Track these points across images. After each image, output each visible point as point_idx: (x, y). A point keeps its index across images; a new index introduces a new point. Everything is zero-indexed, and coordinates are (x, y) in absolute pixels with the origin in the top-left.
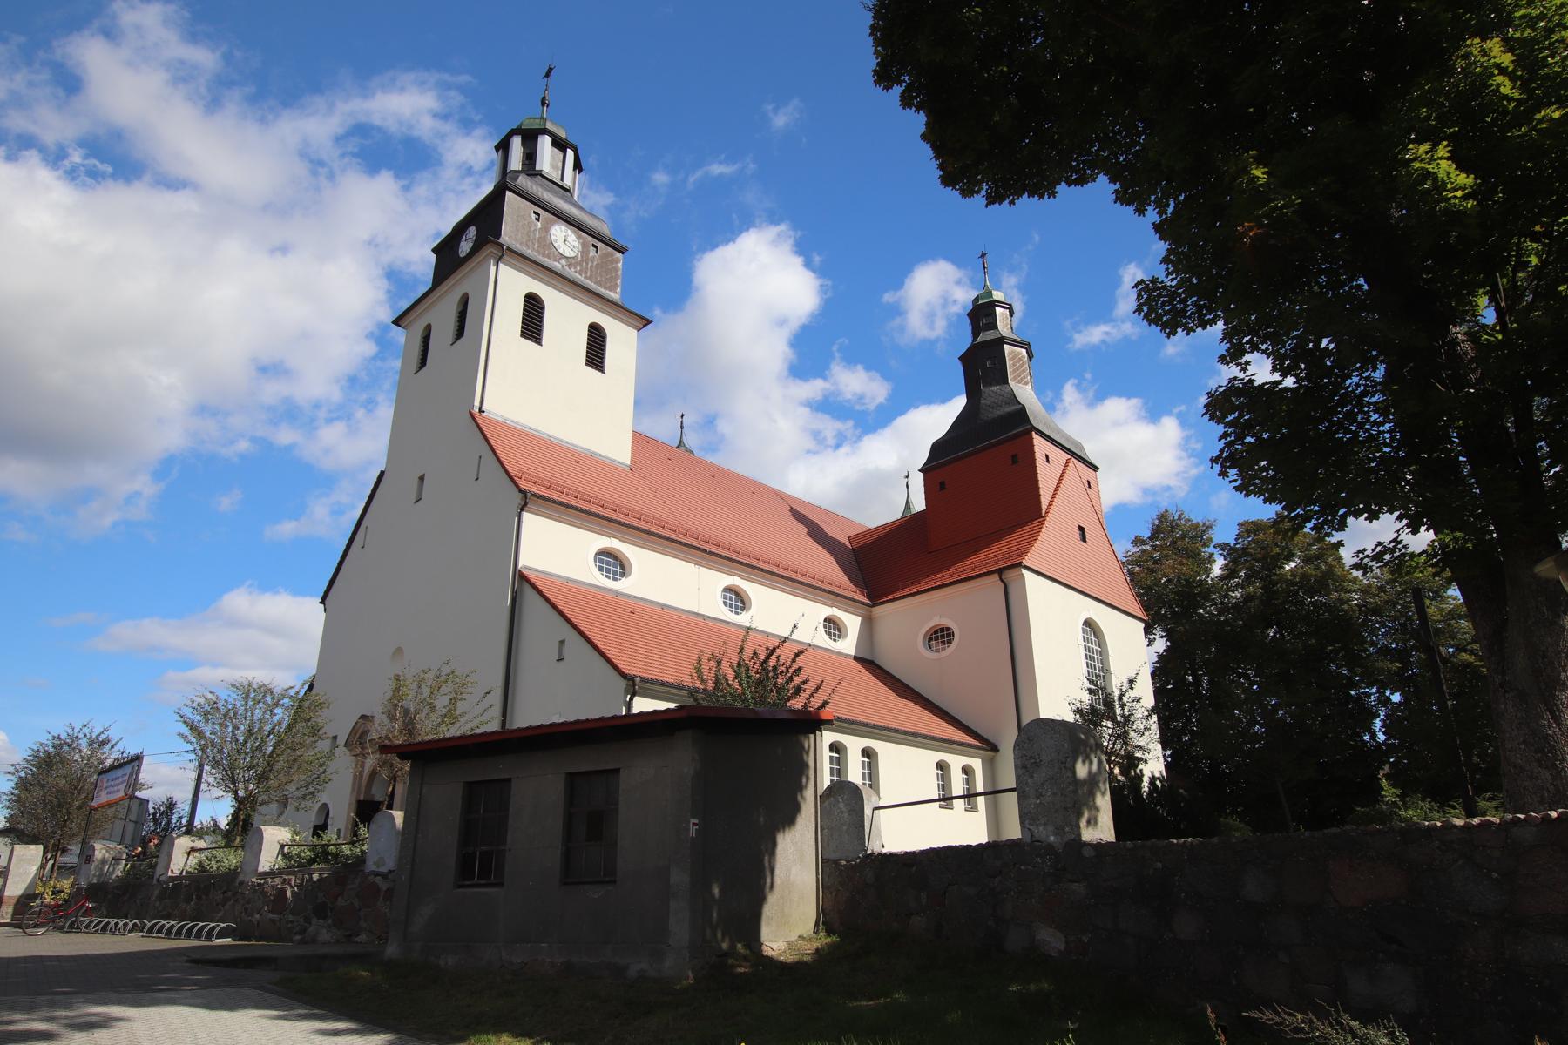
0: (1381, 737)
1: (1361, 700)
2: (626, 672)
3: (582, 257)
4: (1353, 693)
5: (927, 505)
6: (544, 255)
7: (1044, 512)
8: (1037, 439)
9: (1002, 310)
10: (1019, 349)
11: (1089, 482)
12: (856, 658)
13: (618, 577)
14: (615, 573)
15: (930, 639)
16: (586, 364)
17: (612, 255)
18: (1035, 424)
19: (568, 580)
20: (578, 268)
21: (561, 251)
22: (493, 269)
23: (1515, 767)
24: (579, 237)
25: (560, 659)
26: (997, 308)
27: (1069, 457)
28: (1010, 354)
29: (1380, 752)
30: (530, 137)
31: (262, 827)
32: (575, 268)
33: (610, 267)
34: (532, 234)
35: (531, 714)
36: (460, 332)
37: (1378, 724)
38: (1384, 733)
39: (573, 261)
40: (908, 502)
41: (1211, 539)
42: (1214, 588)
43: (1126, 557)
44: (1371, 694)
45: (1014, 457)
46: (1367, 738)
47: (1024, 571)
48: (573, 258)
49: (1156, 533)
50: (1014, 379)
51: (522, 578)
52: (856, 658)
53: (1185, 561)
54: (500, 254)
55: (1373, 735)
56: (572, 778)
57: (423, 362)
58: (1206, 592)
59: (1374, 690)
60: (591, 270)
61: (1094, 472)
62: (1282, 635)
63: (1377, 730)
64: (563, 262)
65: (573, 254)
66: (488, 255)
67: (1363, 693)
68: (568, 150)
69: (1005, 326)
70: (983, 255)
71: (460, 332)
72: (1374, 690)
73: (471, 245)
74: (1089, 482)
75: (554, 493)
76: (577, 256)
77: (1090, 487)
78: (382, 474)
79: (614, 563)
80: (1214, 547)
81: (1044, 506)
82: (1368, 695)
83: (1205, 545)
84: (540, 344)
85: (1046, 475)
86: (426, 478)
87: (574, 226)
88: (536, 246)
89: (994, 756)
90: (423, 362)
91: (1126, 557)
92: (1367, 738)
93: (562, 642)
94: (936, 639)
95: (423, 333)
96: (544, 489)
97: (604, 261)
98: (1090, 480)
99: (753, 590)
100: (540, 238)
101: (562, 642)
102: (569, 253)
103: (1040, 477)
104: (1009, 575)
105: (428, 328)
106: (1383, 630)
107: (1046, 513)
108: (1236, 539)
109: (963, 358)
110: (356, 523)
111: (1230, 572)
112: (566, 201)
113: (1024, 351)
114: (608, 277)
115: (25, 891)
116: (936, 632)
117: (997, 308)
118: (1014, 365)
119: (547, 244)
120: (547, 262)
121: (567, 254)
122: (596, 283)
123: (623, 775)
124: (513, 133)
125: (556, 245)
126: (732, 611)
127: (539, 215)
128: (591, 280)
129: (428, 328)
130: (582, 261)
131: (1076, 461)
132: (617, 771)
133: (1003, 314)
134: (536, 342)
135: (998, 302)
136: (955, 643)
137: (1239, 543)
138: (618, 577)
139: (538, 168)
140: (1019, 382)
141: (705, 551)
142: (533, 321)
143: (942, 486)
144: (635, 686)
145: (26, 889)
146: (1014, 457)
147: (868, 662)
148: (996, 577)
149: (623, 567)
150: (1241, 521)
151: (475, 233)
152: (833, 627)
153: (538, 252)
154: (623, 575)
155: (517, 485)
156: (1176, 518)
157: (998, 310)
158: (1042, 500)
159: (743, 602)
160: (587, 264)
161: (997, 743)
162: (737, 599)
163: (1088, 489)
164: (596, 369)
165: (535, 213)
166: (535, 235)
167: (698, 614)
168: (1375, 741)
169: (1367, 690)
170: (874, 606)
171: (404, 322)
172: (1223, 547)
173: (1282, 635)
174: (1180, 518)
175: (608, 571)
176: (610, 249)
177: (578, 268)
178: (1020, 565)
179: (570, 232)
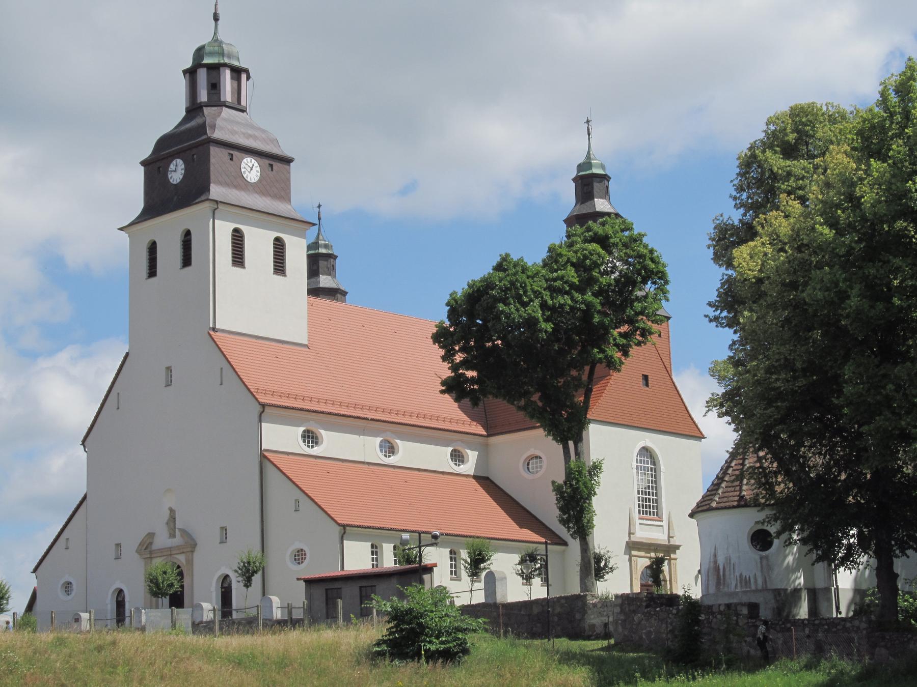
2: (340, 522)
12: (475, 477)
23: (155, 659)
31: (202, 603)
36: (187, 261)
40: (589, 152)
51: (264, 458)
52: (475, 477)
56: (361, 588)
70: (588, 122)
71: (187, 261)
78: (127, 354)
89: (564, 551)
123: (377, 587)
132: (375, 586)
134: (241, 267)
139: (222, 99)
141: (367, 419)
147: (485, 481)
151: (183, 166)
152: (458, 457)
155: (256, 399)
161: (566, 540)
170: (489, 436)
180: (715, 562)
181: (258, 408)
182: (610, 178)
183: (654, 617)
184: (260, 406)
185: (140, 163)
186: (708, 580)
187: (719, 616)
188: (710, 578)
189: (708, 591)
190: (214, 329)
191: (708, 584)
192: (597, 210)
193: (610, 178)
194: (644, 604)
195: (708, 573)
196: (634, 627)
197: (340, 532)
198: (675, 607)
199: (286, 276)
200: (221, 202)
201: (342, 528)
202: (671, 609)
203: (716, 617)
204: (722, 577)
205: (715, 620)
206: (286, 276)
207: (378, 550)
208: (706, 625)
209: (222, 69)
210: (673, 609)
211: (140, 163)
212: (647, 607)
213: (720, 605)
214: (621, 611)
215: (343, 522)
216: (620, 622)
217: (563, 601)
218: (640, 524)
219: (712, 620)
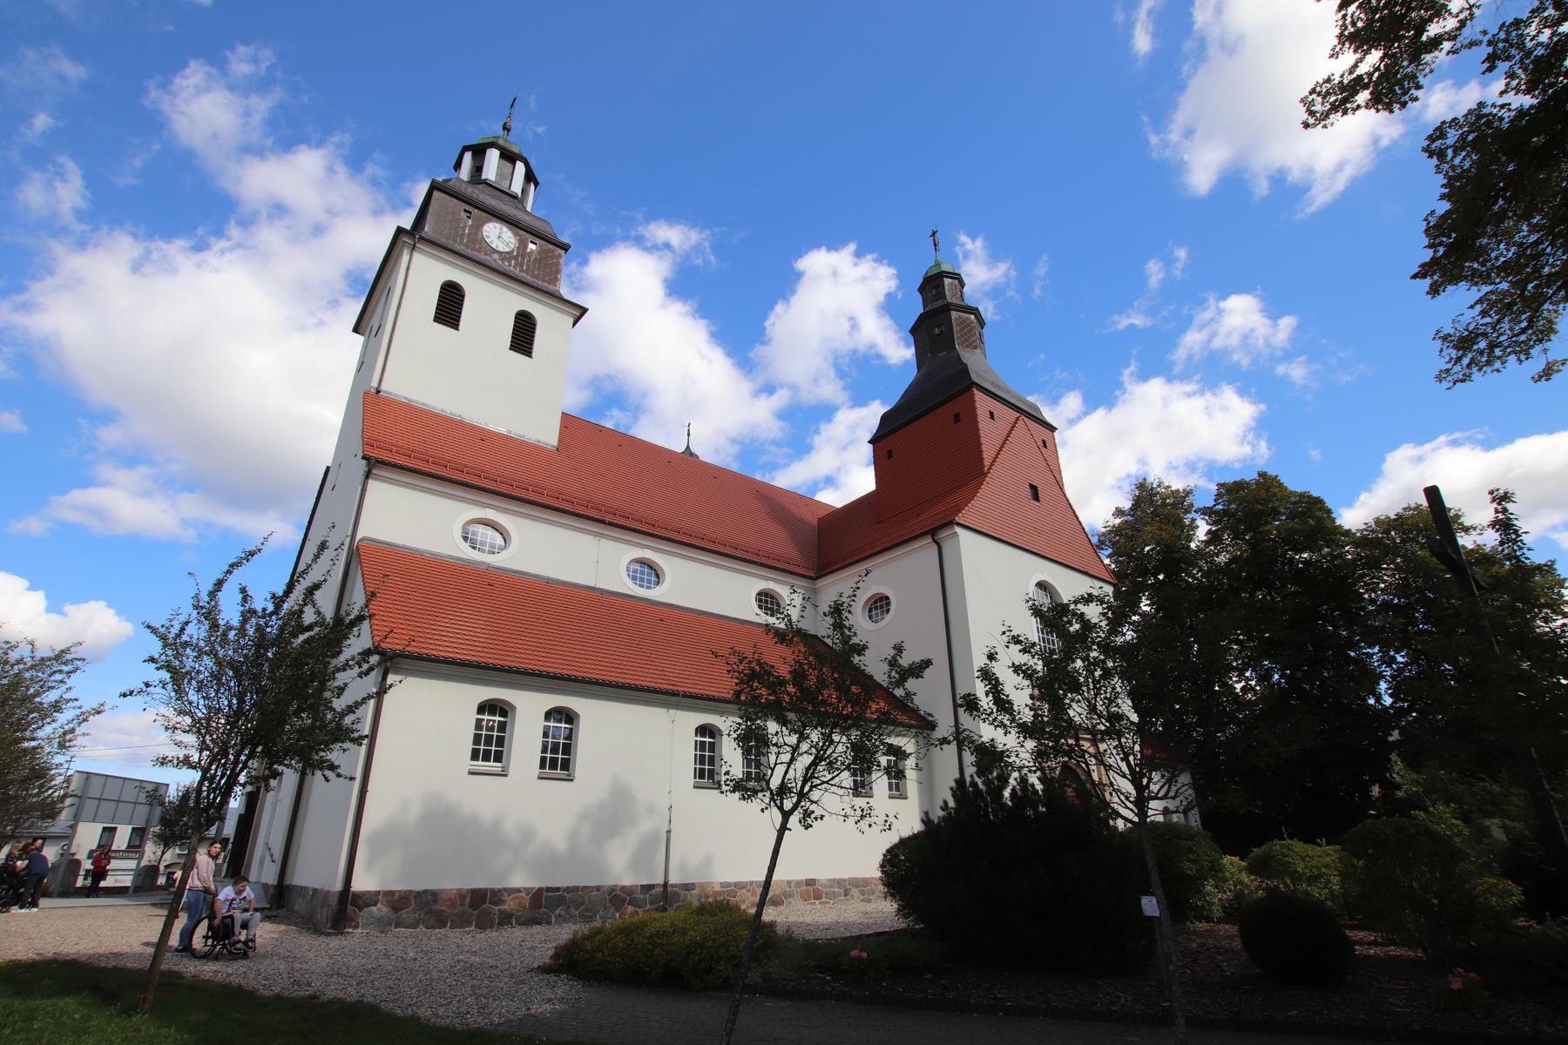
0: (1388, 701)
1: (1362, 663)
3: (518, 252)
4: (1352, 654)
6: (473, 249)
7: (986, 469)
8: (978, 395)
9: (950, 280)
10: (967, 315)
11: (1044, 442)
13: (652, 586)
14: (649, 581)
15: (870, 610)
16: (435, 321)
17: (553, 251)
18: (975, 378)
19: (404, 547)
20: (513, 262)
21: (494, 246)
22: (405, 258)
24: (516, 234)
26: (945, 279)
27: (1019, 415)
28: (957, 319)
29: (1385, 718)
30: (479, 151)
32: (510, 262)
33: (550, 262)
34: (461, 230)
37: (1383, 685)
38: (1391, 695)
39: (508, 256)
41: (1192, 504)
42: (1199, 553)
43: (1105, 527)
44: (1373, 654)
45: (957, 416)
46: (1371, 701)
47: (958, 529)
48: (507, 253)
49: (1137, 503)
50: (962, 343)
53: (1164, 527)
55: (1378, 698)
58: (1192, 558)
59: (1376, 649)
60: (528, 265)
61: (1050, 432)
62: (1271, 596)
63: (1383, 692)
64: (496, 256)
65: (507, 250)
67: (1364, 654)
68: (518, 162)
69: (953, 295)
70: (934, 234)
72: (1376, 649)
74: (1044, 442)
75: (433, 466)
76: (513, 251)
77: (1045, 446)
78: (328, 469)
79: (652, 572)
80: (1195, 512)
81: (987, 463)
82: (1370, 656)
83: (1187, 511)
84: (530, 357)
85: (990, 434)
87: (511, 224)
88: (465, 241)
91: (1105, 527)
92: (1371, 701)
94: (876, 608)
96: (460, 474)
97: (544, 256)
98: (1045, 439)
99: (667, 562)
100: (469, 233)
102: (502, 248)
103: (982, 433)
104: (942, 534)
106: (1382, 586)
107: (989, 469)
108: (1215, 500)
109: (919, 290)
111: (1214, 538)
112: (516, 208)
113: (972, 317)
114: (548, 271)
116: (875, 602)
117: (945, 279)
118: (961, 330)
119: (477, 239)
120: (481, 257)
121: (501, 249)
122: (533, 276)
124: (465, 149)
125: (488, 240)
126: (636, 584)
127: (470, 213)
128: (527, 274)
130: (518, 256)
131: (1026, 419)
133: (951, 284)
135: (945, 272)
136: (893, 607)
137: (1219, 504)
138: (652, 586)
140: (967, 346)
146: (957, 416)
148: (929, 540)
149: (657, 576)
150: (1222, 482)
153: (467, 247)
156: (1155, 486)
157: (947, 281)
158: (985, 456)
159: (657, 576)
160: (523, 258)
162: (652, 572)
163: (1043, 450)
164: (452, 327)
165: (465, 211)
166: (464, 231)
168: (1382, 704)
169: (1369, 650)
172: (1206, 511)
173: (1271, 596)
174: (1159, 486)
175: (642, 580)
176: (551, 246)
177: (513, 262)
178: (951, 523)
179: (505, 229)
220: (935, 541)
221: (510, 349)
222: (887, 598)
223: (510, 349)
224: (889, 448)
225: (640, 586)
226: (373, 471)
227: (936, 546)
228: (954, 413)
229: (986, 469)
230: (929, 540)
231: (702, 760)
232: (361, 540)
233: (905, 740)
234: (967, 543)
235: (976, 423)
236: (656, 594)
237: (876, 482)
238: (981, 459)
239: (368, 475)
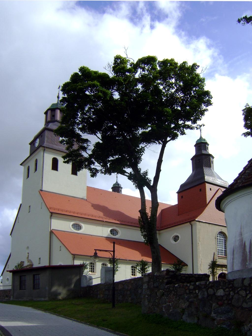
5: (178, 203)
25: (60, 250)
35: (56, 263)
54: (44, 149)
57: (28, 177)
66: (41, 150)
73: (38, 144)
78: (21, 205)
79: (78, 227)
86: (31, 206)
90: (28, 177)
93: (61, 247)
95: (35, 162)
101: (61, 247)
104: (193, 223)
105: (29, 167)
109: (192, 159)
110: (15, 219)
115: (5, 326)
116: (176, 237)
129: (29, 167)
138: (79, 229)
139: (56, 119)
142: (55, 166)
143: (182, 197)
144: (75, 256)
145: (7, 326)
146: (200, 190)
149: (117, 232)
151: (39, 141)
154: (80, 229)
167: (102, 237)
171: (23, 164)
178: (194, 220)
180: (242, 240)
181: (50, 214)
182: (214, 157)
183: (173, 292)
184: (50, 213)
185: (29, 144)
186: (233, 259)
187: (243, 293)
188: (236, 256)
189: (233, 269)
190: (42, 190)
191: (233, 262)
192: (203, 153)
193: (214, 157)
194: (165, 281)
195: (233, 251)
196: (157, 301)
197: (72, 257)
198: (192, 283)
199: (77, 175)
200: (46, 147)
201: (73, 255)
202: (188, 285)
203: (238, 293)
204: (248, 253)
205: (236, 296)
206: (77, 175)
207: (94, 265)
208: (226, 302)
209: (56, 110)
210: (190, 285)
211: (29, 144)
212: (167, 283)
213: (243, 279)
214: (148, 287)
215: (74, 253)
216: (147, 296)
217: (133, 282)
218: (218, 258)
219: (233, 296)
220: (190, 224)
221: (72, 174)
222: (178, 236)
223: (72, 174)
224: (182, 196)
225: (113, 235)
226: (53, 215)
227: (191, 225)
228: (200, 188)
229: (207, 203)
230: (189, 223)
231: (132, 272)
232: (52, 230)
233: (78, 132)
234: (198, 227)
235: (205, 192)
236: (116, 237)
237: (178, 199)
238: (206, 202)
239: (51, 216)
